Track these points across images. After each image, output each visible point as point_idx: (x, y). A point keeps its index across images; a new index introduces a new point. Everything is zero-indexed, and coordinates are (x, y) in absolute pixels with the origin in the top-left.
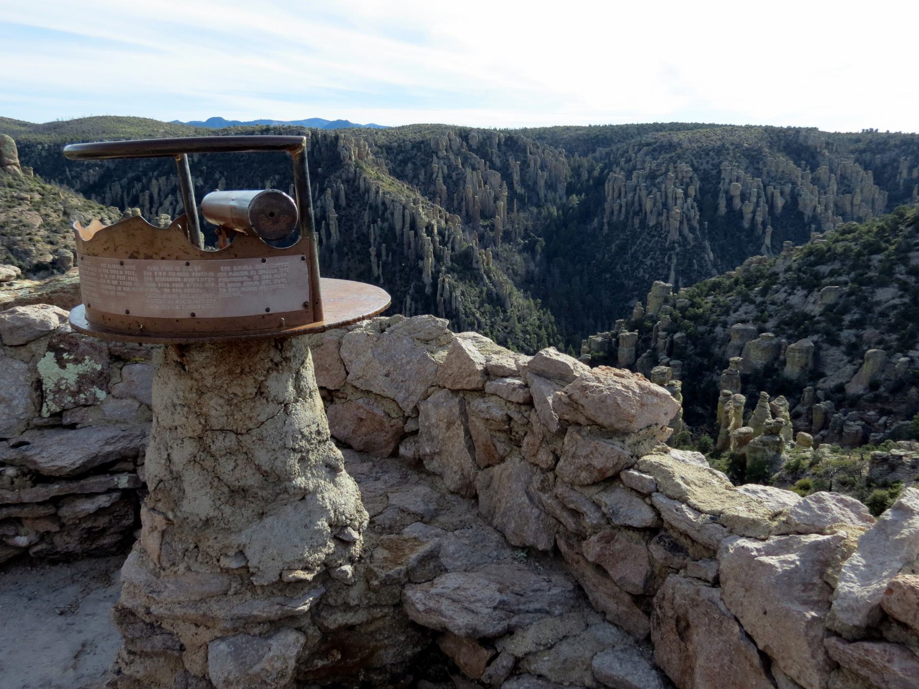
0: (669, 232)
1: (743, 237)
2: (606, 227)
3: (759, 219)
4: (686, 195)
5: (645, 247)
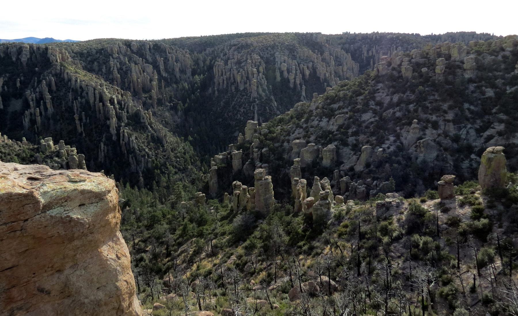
1: (291, 92)
2: (216, 93)
3: (298, 82)
4: (259, 72)
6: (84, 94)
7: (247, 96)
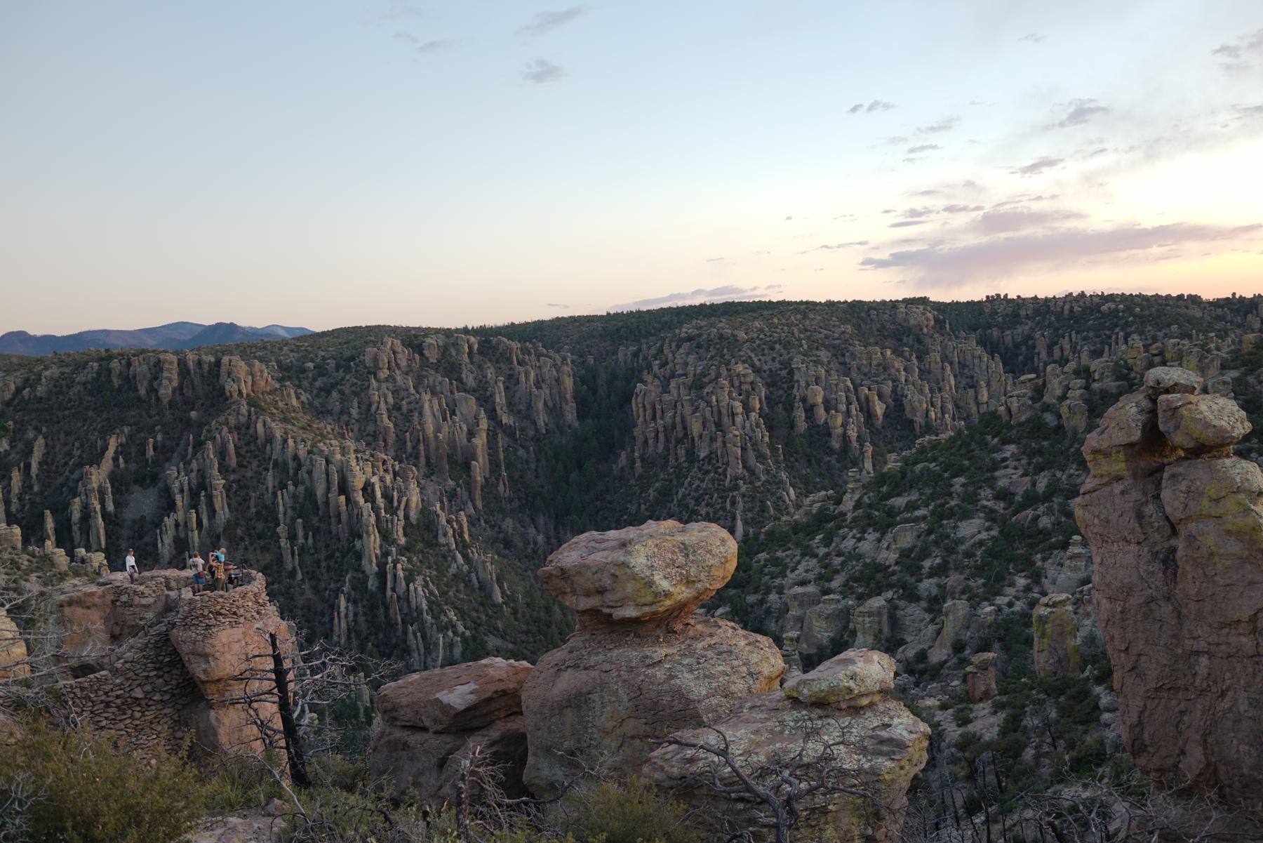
0: (727, 464)
1: (834, 462)
2: (638, 464)
3: (853, 433)
4: (747, 408)
5: (696, 490)
6: (303, 474)
7: (716, 472)
